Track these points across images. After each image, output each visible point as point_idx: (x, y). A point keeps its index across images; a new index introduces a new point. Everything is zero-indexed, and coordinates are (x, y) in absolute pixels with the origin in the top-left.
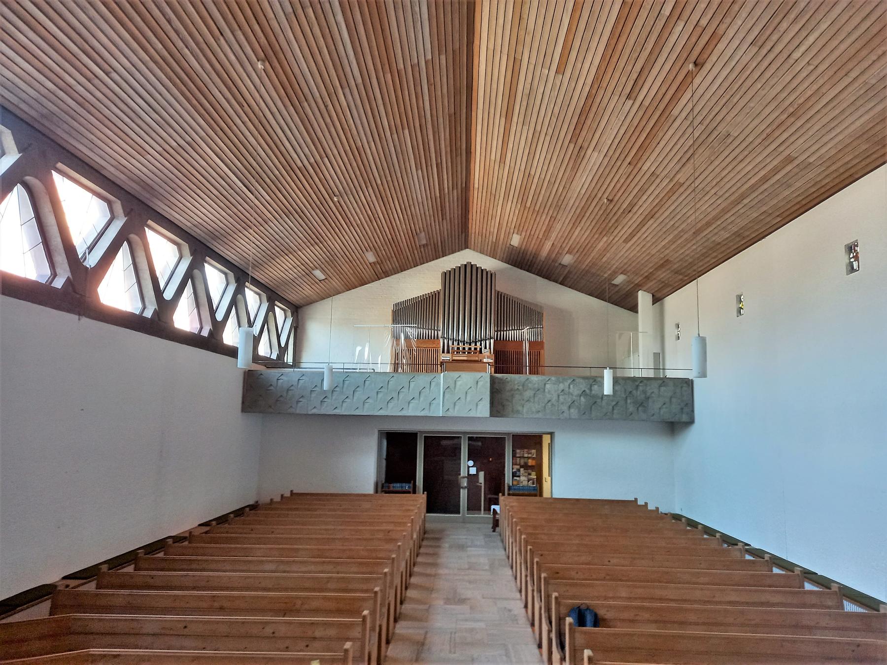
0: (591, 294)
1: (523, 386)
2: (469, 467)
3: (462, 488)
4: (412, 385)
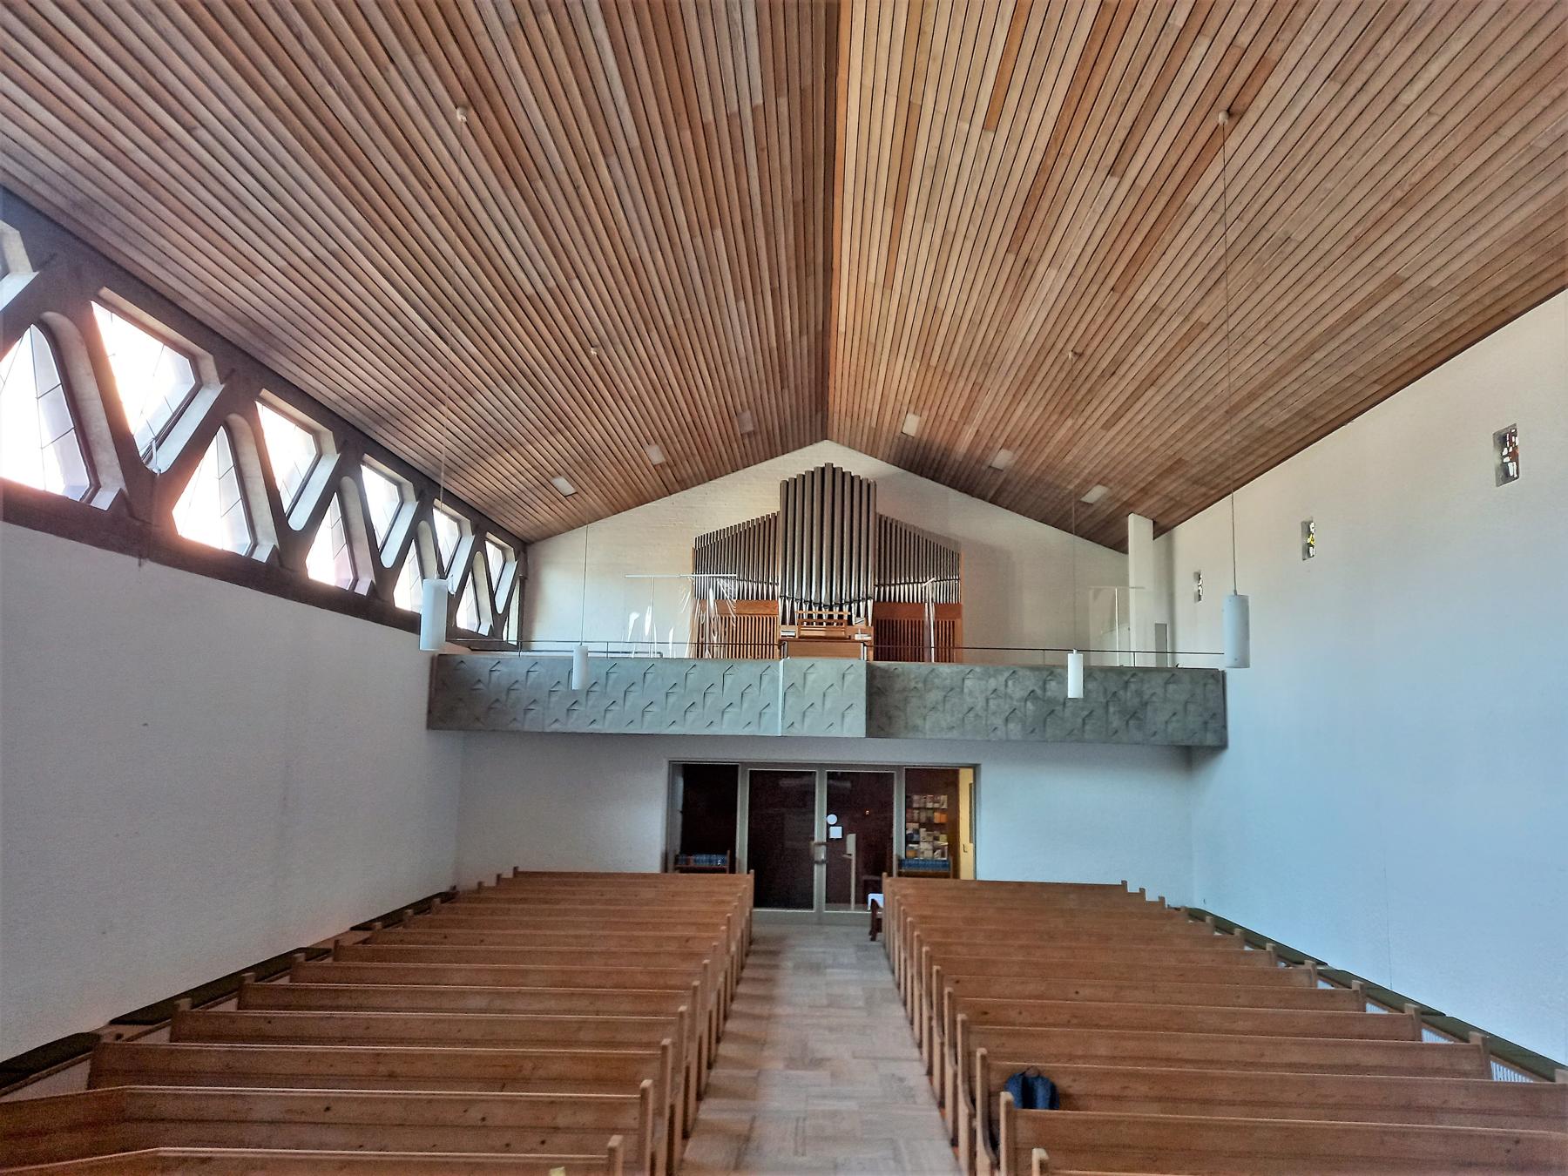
0: (1044, 521)
1: (925, 682)
2: (829, 826)
3: (817, 862)
4: (728, 680)
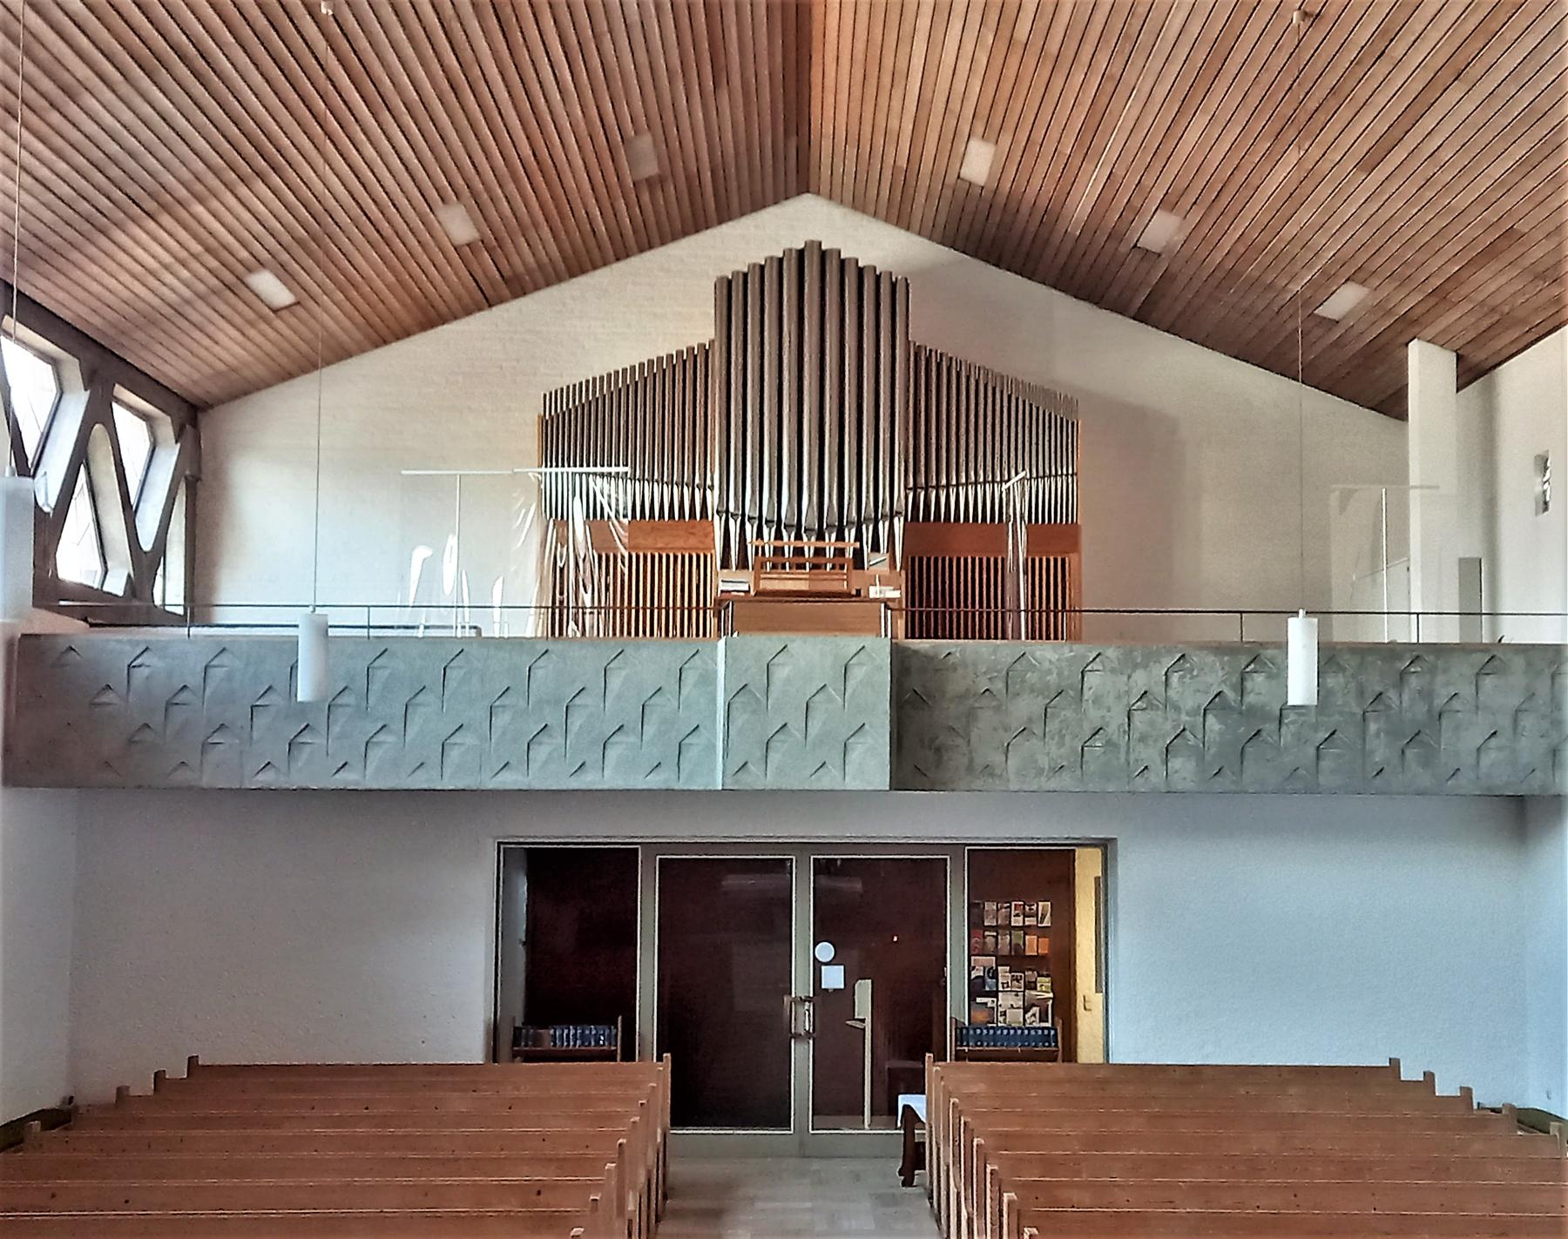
2: (818, 964)
3: (797, 1036)
4: (615, 683)
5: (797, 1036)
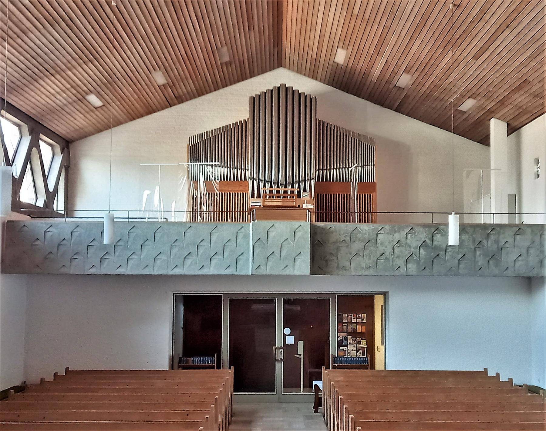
2: (285, 335)
3: (278, 360)
4: (214, 237)
5: (278, 360)
